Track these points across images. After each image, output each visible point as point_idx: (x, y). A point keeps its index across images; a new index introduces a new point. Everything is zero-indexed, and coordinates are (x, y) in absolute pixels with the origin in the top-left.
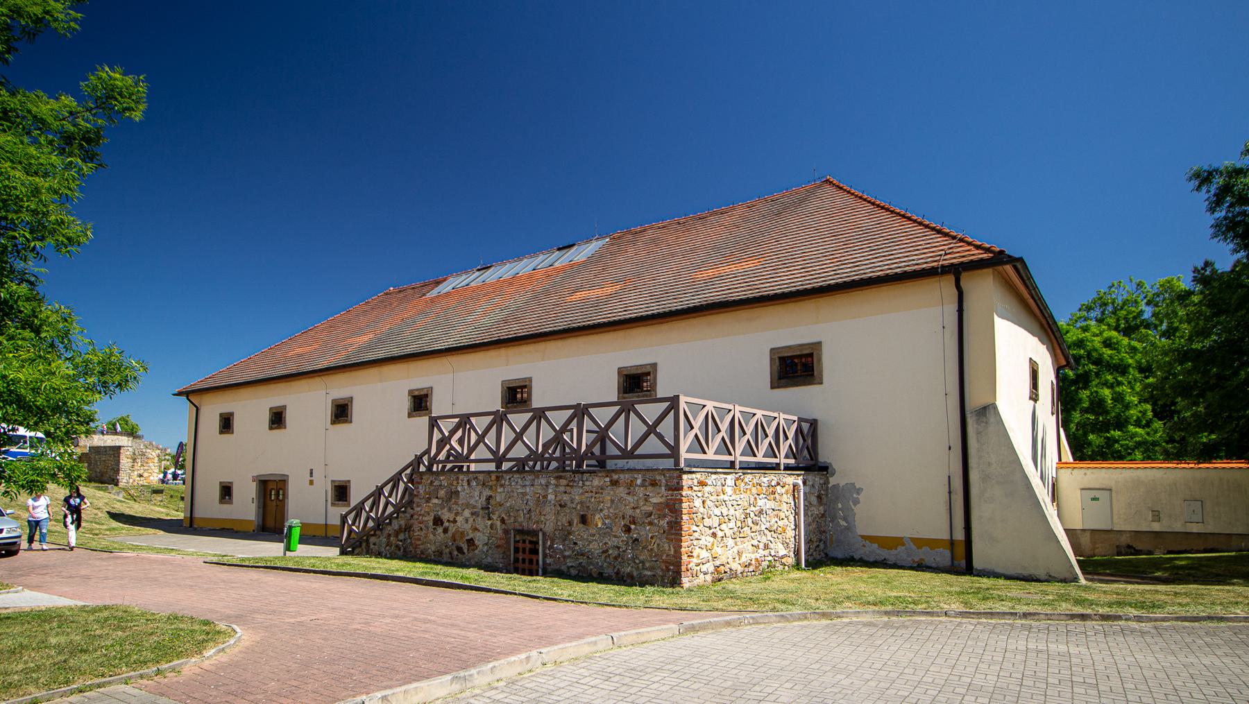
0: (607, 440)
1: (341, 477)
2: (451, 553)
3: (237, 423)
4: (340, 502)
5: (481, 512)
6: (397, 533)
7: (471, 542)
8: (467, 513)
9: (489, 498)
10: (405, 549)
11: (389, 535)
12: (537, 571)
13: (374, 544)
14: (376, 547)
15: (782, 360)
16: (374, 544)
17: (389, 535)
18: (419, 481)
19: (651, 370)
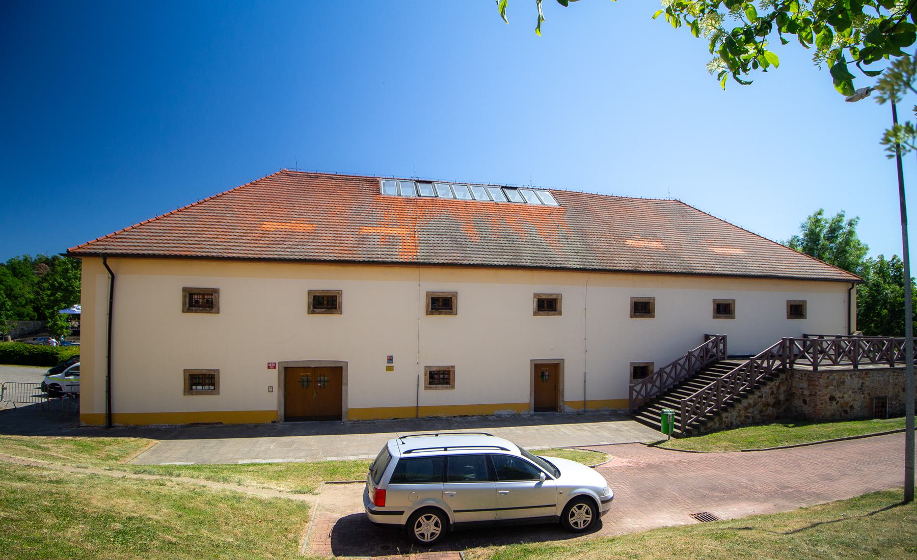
0: (794, 345)
2: (840, 414)
5: (858, 391)
6: (746, 409)
7: (852, 407)
8: (850, 392)
9: (863, 383)
10: (753, 417)
11: (740, 410)
12: (886, 415)
13: (727, 418)
14: (728, 419)
15: (791, 306)
16: (727, 418)
17: (740, 410)
18: (820, 377)
19: (732, 303)
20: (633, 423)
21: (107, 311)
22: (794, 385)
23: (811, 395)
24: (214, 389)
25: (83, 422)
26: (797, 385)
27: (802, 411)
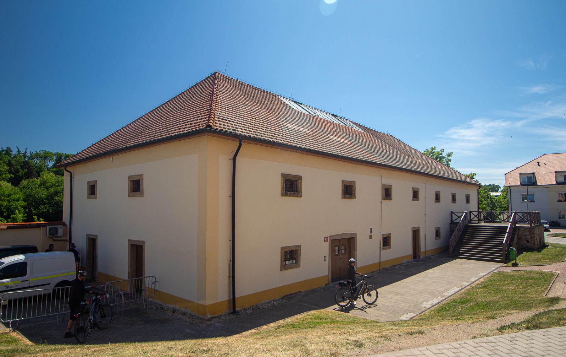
1: (386, 232)
3: (146, 185)
4: (386, 247)
20: (458, 260)
21: (228, 192)
22: (520, 234)
23: (531, 238)
24: (295, 263)
25: (208, 314)
26: (522, 234)
27: (526, 246)
